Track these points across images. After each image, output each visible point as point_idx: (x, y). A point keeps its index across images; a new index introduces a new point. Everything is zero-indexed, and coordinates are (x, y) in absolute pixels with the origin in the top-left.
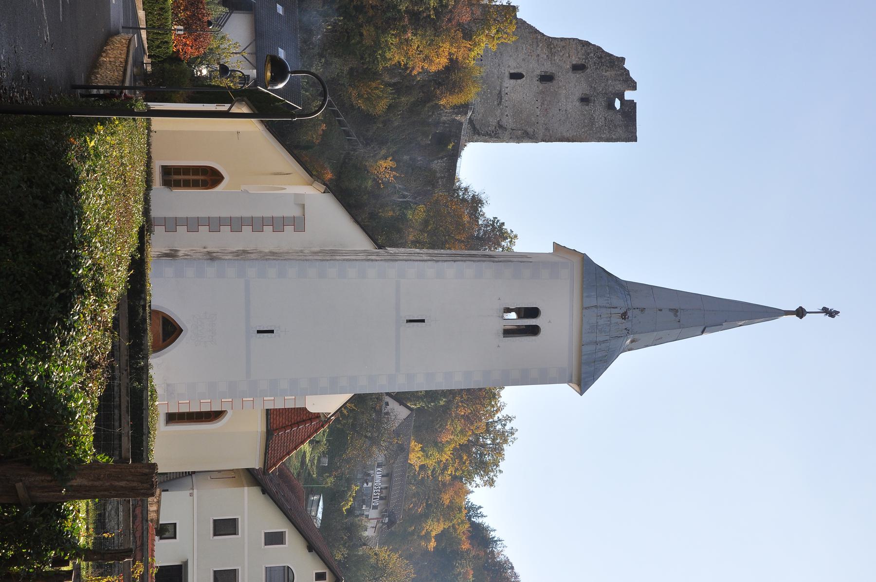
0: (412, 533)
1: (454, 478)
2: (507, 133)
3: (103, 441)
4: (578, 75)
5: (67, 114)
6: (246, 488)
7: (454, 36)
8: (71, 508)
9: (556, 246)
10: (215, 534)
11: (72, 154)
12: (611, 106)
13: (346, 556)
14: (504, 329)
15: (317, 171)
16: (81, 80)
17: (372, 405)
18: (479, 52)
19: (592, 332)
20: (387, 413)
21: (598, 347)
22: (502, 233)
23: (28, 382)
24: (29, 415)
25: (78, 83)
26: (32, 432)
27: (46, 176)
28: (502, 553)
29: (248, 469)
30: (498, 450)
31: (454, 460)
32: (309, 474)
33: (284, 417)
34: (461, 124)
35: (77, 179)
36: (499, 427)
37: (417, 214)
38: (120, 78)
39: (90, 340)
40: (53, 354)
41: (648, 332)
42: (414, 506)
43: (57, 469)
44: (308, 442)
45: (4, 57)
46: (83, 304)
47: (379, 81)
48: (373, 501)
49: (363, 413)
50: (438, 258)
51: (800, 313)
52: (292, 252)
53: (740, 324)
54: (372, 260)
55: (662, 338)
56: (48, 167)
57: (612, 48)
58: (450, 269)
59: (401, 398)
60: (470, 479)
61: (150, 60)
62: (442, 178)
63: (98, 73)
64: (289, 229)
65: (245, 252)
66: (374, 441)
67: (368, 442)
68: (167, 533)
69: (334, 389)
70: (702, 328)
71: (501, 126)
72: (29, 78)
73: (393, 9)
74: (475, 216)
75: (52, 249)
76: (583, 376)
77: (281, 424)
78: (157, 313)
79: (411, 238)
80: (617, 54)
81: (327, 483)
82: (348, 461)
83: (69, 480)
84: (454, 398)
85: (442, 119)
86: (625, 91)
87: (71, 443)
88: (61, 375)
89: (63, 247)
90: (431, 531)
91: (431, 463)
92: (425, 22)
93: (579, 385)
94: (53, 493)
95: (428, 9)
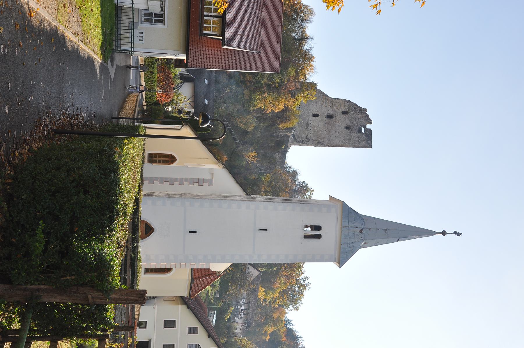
0: (258, 332)
1: (280, 306)
2: (310, 142)
3: (123, 281)
4: (345, 116)
5: (113, 136)
6: (180, 306)
7: (287, 96)
8: (110, 307)
9: (330, 197)
10: (165, 327)
11: (116, 156)
12: (360, 131)
13: (226, 341)
14: (304, 236)
15: (220, 157)
16: (115, 115)
17: (241, 269)
18: (298, 104)
19: (346, 239)
20: (249, 273)
21: (349, 245)
22: (307, 189)
23: (94, 253)
24: (95, 267)
25: (114, 116)
26: (96, 274)
27: (106, 165)
28: (302, 343)
29: (181, 297)
30: (301, 293)
31: (280, 297)
32: (210, 300)
33: (199, 272)
34: (289, 137)
35: (118, 167)
36: (302, 282)
37: (267, 178)
38: (133, 114)
39: (120, 235)
40: (105, 241)
41: (371, 240)
42: (260, 319)
43: (106, 290)
44: (210, 285)
45: (86, 107)
46: (119, 220)
47: (251, 115)
48: (240, 315)
49: (237, 272)
50: (275, 201)
51: (444, 233)
52: (207, 195)
53: (416, 237)
54: (244, 201)
55: (379, 242)
56: (107, 161)
57: (361, 104)
58: (280, 206)
59: (255, 266)
60: (287, 307)
61: (145, 104)
62: (279, 161)
63: (123, 111)
64: (206, 184)
65: (185, 194)
66: (242, 286)
67: (239, 287)
68: (142, 325)
69: (223, 261)
70: (398, 239)
71: (307, 138)
72: (95, 115)
73: (259, 82)
74: (294, 180)
75: (107, 196)
76: (341, 259)
77: (198, 276)
78: (143, 221)
79: (263, 189)
80: (363, 107)
81: (218, 306)
82: (229, 295)
83: (110, 295)
84: (281, 267)
85: (280, 134)
86: (366, 124)
87: (111, 280)
88: (108, 250)
89: (112, 196)
90: (268, 331)
91: (268, 298)
92: (274, 89)
93: (339, 263)
94: (103, 301)
95: (275, 83)
